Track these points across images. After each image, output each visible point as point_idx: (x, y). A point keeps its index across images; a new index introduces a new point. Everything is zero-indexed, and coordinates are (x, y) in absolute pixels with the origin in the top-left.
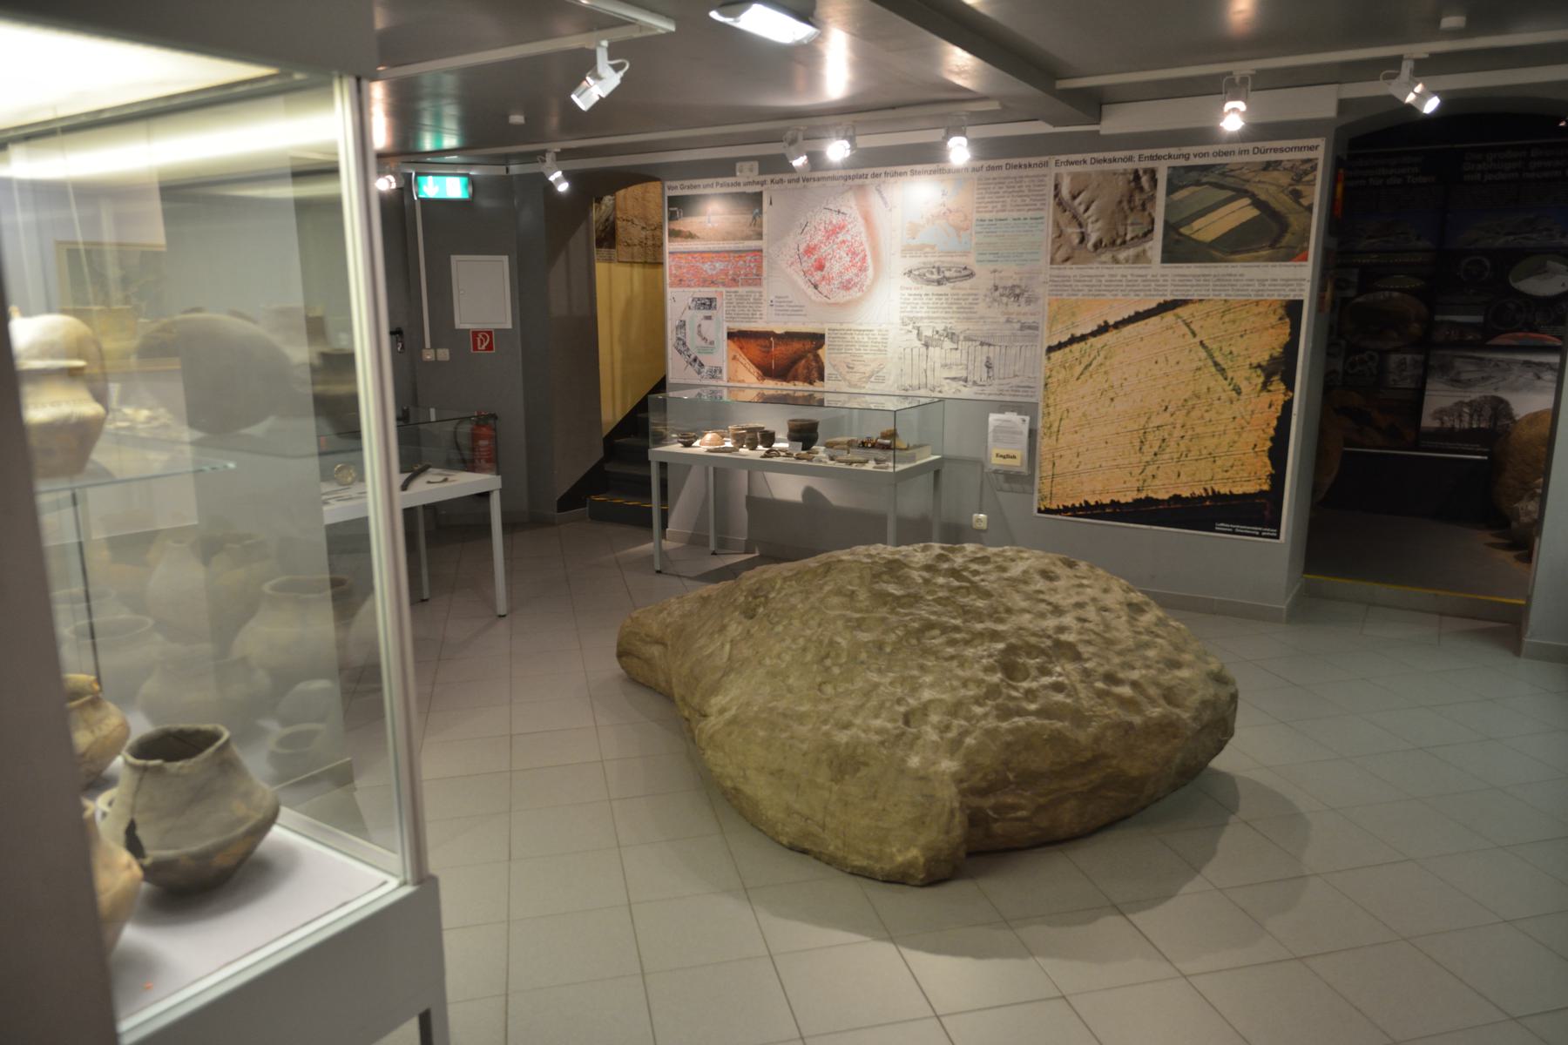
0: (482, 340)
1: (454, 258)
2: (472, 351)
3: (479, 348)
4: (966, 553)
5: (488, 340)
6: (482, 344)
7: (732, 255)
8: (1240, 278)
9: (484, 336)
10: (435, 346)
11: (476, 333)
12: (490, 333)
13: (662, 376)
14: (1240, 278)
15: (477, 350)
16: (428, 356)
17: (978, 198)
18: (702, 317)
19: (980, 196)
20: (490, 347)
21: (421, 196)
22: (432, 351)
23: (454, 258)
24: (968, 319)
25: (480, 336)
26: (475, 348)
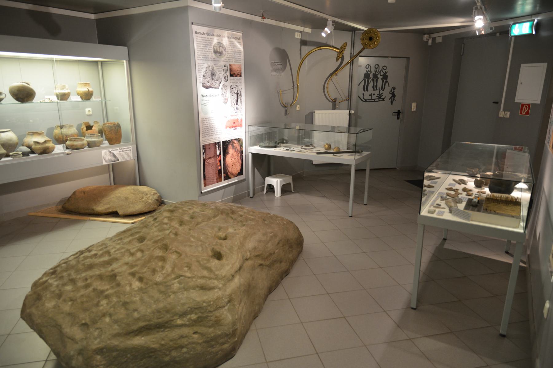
0: (525, 109)
1: (545, 65)
2: (519, 114)
3: (523, 113)
4: (53, 289)
5: (527, 110)
6: (524, 111)
7: (214, 86)
8: (203, 130)
9: (526, 107)
10: (505, 110)
11: (523, 105)
12: (529, 105)
13: (35, 152)
14: (203, 130)
15: (522, 114)
16: (502, 114)
17: (212, 41)
18: (93, 128)
19: (212, 40)
20: (527, 113)
21: (512, 35)
22: (503, 112)
23: (545, 65)
24: (218, 137)
25: (524, 106)
26: (521, 113)
